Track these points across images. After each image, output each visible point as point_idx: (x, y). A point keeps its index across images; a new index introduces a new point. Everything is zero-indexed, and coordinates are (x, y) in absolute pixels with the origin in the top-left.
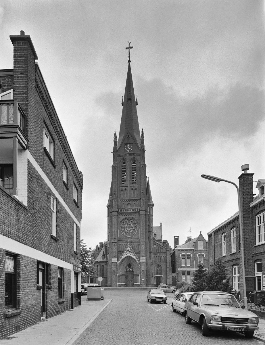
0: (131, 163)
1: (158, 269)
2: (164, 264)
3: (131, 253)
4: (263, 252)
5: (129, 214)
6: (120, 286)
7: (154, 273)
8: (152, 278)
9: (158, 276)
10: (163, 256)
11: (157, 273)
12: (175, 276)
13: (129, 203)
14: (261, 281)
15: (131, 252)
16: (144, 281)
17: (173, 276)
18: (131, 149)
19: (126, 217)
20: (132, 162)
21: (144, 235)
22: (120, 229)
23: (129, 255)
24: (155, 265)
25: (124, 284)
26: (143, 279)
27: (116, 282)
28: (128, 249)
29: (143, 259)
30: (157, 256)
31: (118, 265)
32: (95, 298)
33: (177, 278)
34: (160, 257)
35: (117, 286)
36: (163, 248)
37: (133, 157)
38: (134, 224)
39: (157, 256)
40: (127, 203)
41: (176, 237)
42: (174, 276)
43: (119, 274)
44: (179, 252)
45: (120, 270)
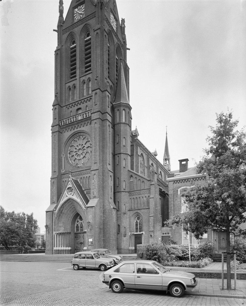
0: (83, 37)
1: (138, 221)
2: (146, 211)
3: (73, 193)
4: (243, 274)
5: (76, 126)
6: (59, 252)
7: (130, 229)
8: (125, 239)
9: (138, 233)
10: (146, 197)
11: (137, 229)
12: (168, 233)
13: (79, 106)
14: (70, 254)
15: (73, 191)
16: (92, 242)
17: (163, 234)
19: (73, 131)
20: (84, 34)
21: (98, 158)
22: (66, 156)
23: (70, 196)
24: (132, 213)
25: (70, 248)
26: (91, 240)
27: (53, 246)
28: (70, 186)
29: (93, 202)
30: (135, 197)
31: (55, 216)
32: (130, 260)
33: (171, 236)
34: (143, 197)
35: (53, 252)
36: (145, 181)
38: (83, 139)
39: (135, 197)
40: (76, 108)
41: (183, 163)
42: (166, 234)
43: (58, 232)
44: (175, 185)
45: (61, 224)
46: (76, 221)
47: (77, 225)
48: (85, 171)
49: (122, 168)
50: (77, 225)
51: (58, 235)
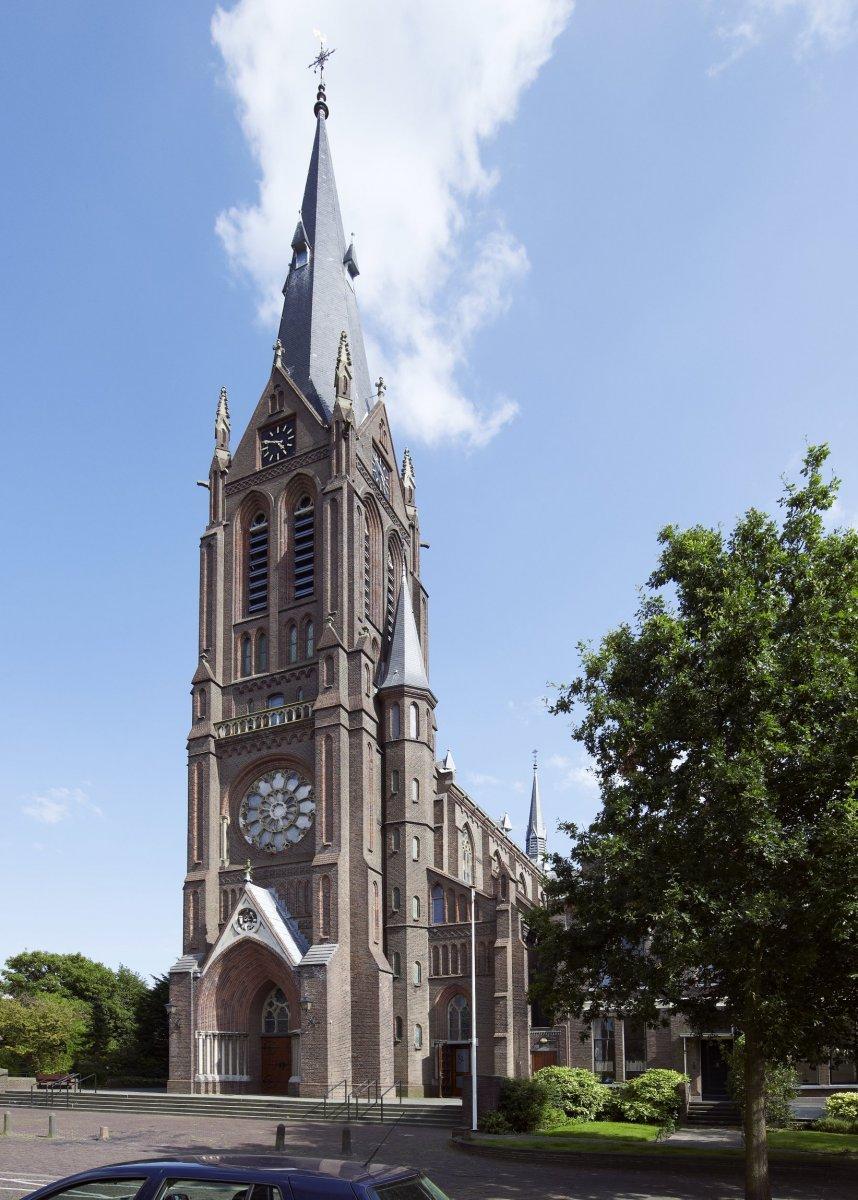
18: (286, 448)
23: (252, 934)
37: (295, 472)
46: (266, 1004)
47: (270, 1014)
48: (293, 866)
49: (409, 861)
50: (270, 1014)
51: (208, 1041)
